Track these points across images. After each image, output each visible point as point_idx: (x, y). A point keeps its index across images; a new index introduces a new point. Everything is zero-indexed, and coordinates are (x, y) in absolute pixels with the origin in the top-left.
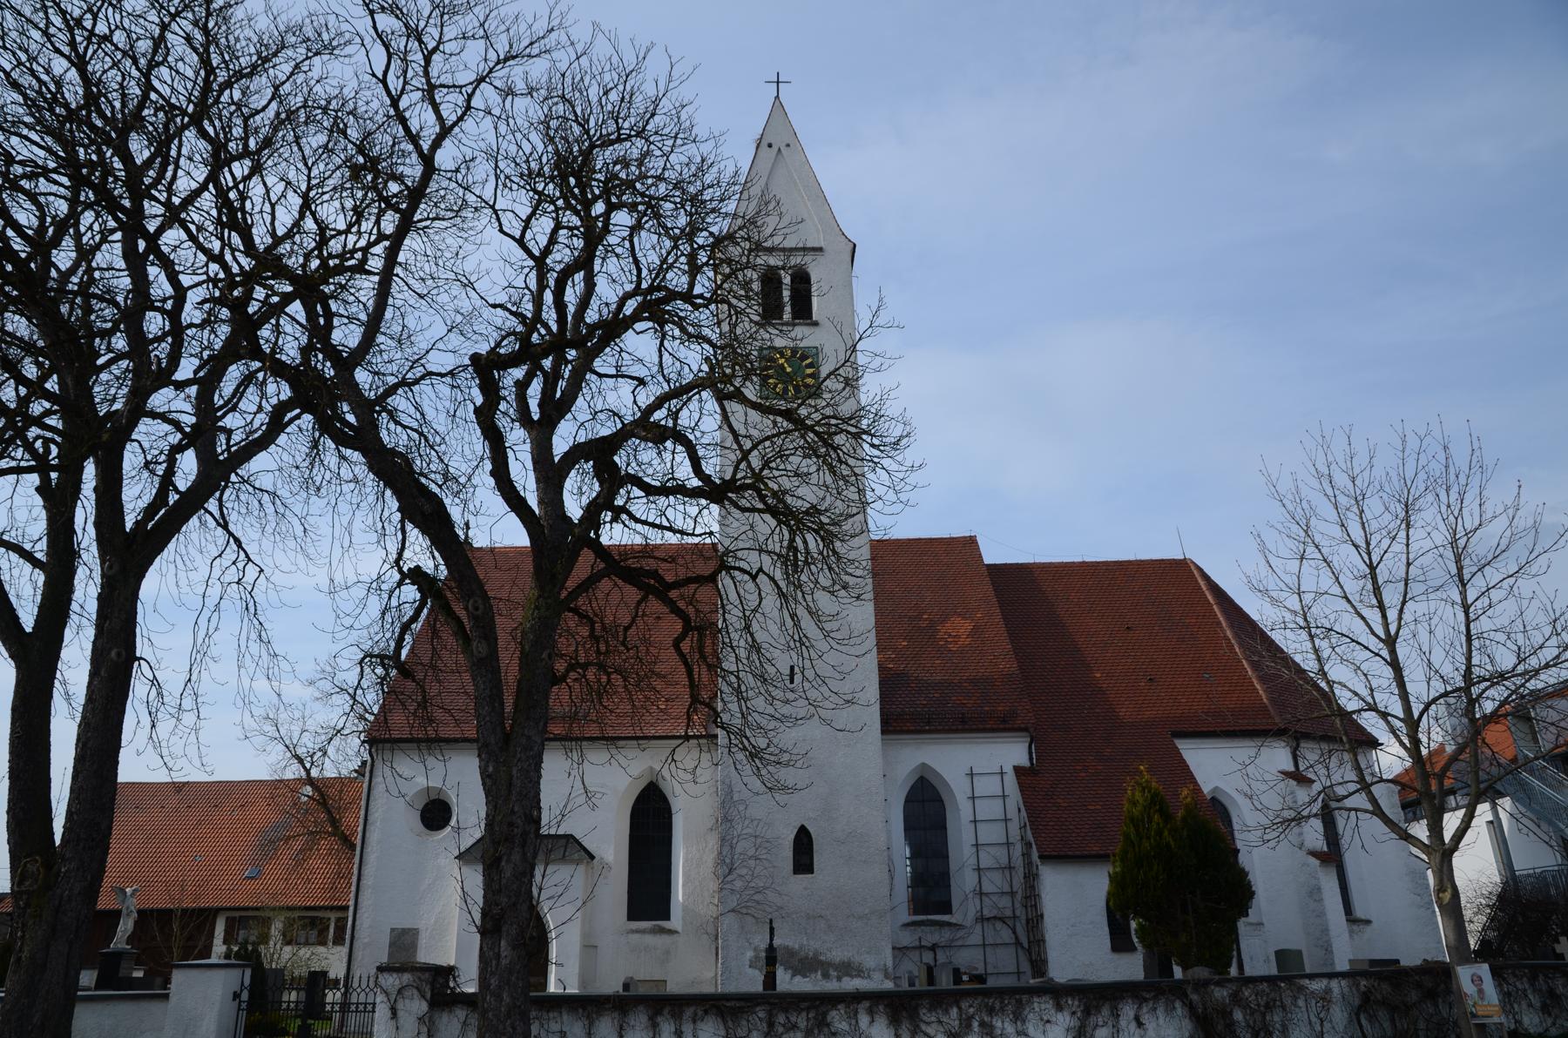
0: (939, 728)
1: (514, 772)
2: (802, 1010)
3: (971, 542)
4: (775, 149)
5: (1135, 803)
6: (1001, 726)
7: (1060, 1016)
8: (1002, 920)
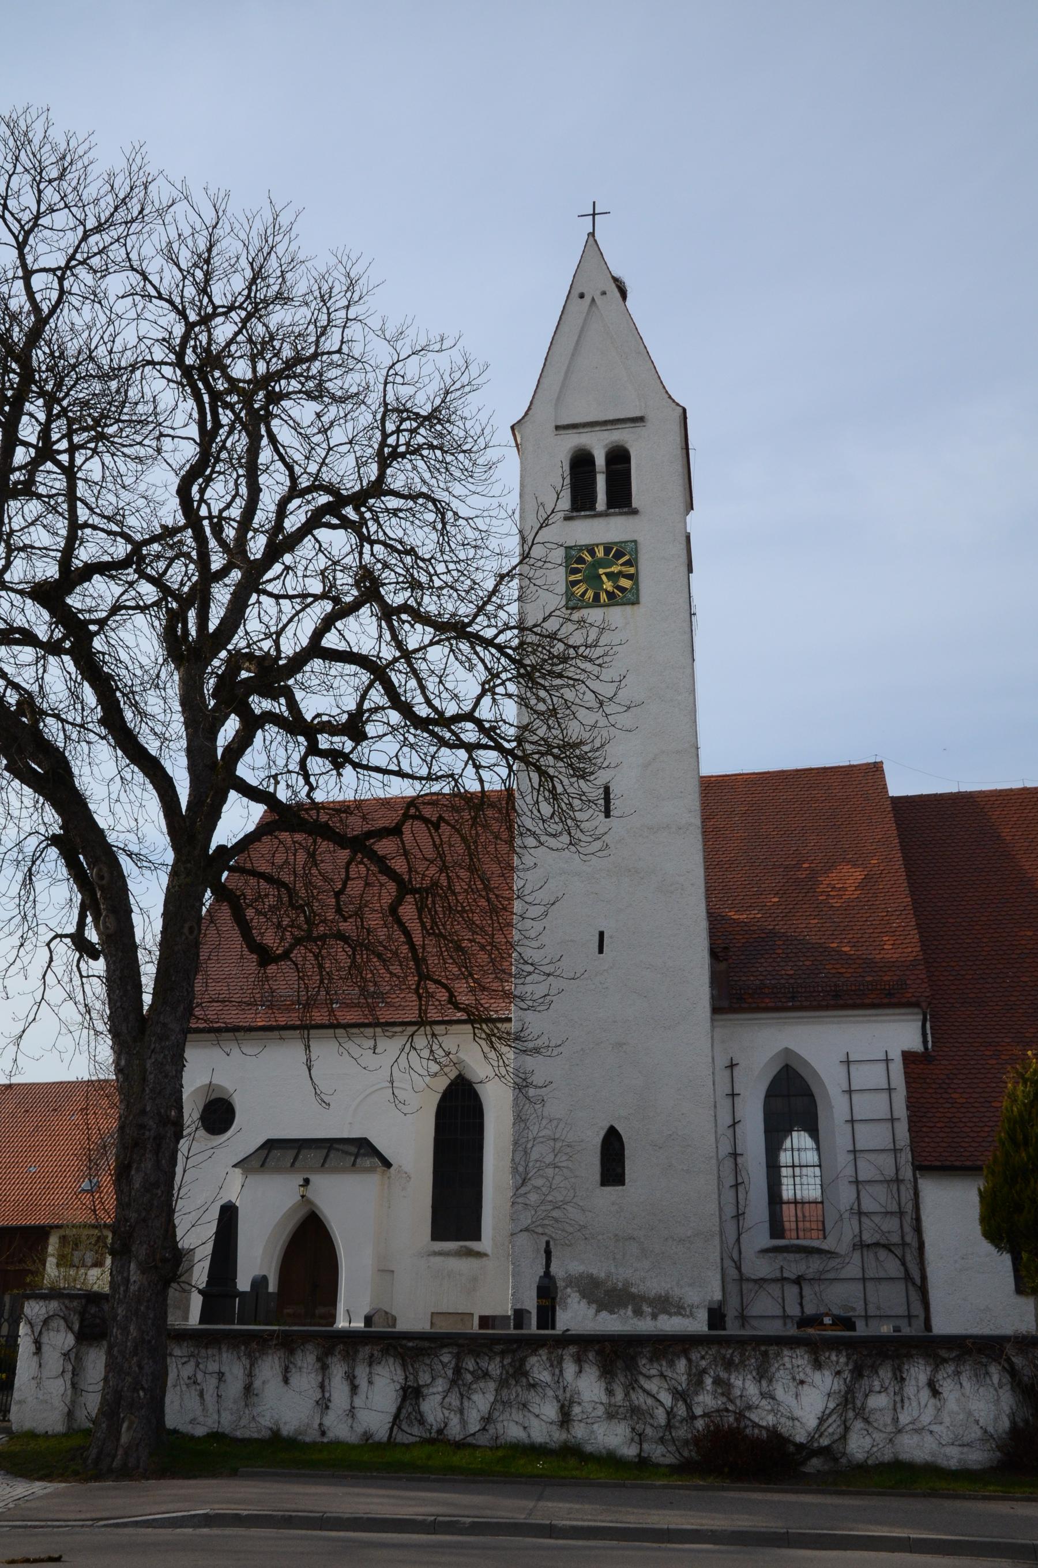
0: (806, 1004)
1: (148, 1065)
2: (496, 1354)
3: (875, 771)
4: (588, 299)
5: (1014, 1100)
6: (886, 1001)
7: (817, 1377)
8: (887, 1247)
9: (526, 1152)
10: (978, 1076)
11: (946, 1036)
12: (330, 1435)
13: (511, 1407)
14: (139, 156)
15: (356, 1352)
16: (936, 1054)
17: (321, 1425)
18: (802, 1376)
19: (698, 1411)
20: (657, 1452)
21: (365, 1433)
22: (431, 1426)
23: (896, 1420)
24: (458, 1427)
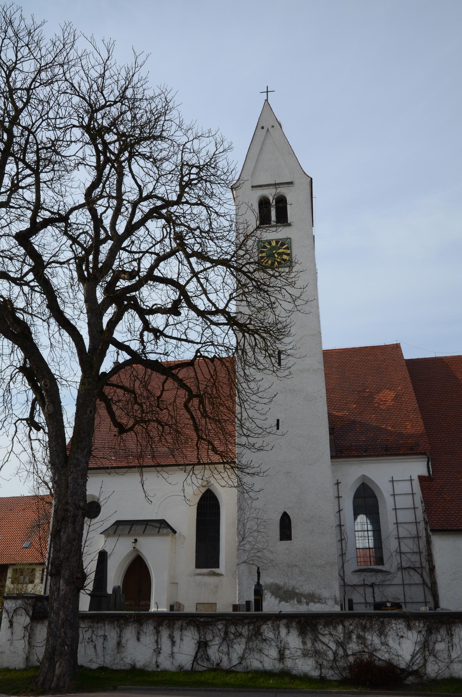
2: (245, 624)
3: (397, 347)
4: (265, 129)
6: (410, 452)
7: (410, 634)
8: (414, 569)
9: (244, 525)
10: (455, 487)
11: (438, 468)
12: (161, 668)
13: (254, 651)
14: (69, 27)
15: (174, 624)
16: (434, 477)
17: (156, 662)
18: (402, 634)
19: (350, 652)
20: (329, 674)
21: (179, 666)
22: (213, 661)
23: (450, 656)
24: (227, 662)
